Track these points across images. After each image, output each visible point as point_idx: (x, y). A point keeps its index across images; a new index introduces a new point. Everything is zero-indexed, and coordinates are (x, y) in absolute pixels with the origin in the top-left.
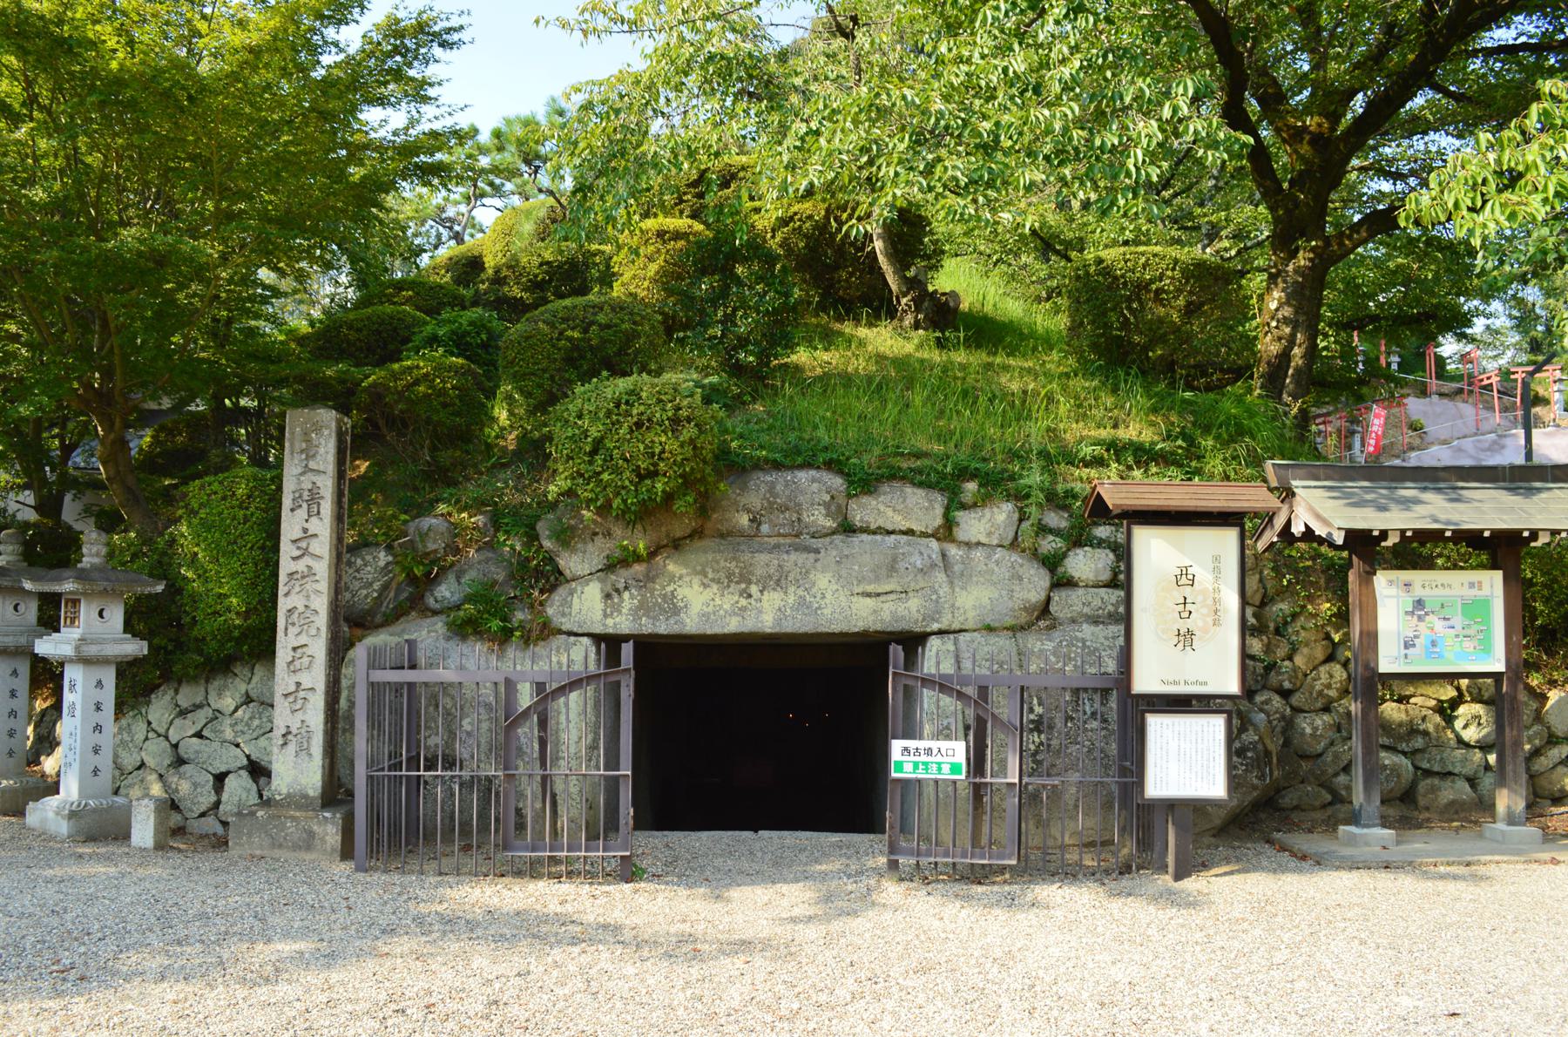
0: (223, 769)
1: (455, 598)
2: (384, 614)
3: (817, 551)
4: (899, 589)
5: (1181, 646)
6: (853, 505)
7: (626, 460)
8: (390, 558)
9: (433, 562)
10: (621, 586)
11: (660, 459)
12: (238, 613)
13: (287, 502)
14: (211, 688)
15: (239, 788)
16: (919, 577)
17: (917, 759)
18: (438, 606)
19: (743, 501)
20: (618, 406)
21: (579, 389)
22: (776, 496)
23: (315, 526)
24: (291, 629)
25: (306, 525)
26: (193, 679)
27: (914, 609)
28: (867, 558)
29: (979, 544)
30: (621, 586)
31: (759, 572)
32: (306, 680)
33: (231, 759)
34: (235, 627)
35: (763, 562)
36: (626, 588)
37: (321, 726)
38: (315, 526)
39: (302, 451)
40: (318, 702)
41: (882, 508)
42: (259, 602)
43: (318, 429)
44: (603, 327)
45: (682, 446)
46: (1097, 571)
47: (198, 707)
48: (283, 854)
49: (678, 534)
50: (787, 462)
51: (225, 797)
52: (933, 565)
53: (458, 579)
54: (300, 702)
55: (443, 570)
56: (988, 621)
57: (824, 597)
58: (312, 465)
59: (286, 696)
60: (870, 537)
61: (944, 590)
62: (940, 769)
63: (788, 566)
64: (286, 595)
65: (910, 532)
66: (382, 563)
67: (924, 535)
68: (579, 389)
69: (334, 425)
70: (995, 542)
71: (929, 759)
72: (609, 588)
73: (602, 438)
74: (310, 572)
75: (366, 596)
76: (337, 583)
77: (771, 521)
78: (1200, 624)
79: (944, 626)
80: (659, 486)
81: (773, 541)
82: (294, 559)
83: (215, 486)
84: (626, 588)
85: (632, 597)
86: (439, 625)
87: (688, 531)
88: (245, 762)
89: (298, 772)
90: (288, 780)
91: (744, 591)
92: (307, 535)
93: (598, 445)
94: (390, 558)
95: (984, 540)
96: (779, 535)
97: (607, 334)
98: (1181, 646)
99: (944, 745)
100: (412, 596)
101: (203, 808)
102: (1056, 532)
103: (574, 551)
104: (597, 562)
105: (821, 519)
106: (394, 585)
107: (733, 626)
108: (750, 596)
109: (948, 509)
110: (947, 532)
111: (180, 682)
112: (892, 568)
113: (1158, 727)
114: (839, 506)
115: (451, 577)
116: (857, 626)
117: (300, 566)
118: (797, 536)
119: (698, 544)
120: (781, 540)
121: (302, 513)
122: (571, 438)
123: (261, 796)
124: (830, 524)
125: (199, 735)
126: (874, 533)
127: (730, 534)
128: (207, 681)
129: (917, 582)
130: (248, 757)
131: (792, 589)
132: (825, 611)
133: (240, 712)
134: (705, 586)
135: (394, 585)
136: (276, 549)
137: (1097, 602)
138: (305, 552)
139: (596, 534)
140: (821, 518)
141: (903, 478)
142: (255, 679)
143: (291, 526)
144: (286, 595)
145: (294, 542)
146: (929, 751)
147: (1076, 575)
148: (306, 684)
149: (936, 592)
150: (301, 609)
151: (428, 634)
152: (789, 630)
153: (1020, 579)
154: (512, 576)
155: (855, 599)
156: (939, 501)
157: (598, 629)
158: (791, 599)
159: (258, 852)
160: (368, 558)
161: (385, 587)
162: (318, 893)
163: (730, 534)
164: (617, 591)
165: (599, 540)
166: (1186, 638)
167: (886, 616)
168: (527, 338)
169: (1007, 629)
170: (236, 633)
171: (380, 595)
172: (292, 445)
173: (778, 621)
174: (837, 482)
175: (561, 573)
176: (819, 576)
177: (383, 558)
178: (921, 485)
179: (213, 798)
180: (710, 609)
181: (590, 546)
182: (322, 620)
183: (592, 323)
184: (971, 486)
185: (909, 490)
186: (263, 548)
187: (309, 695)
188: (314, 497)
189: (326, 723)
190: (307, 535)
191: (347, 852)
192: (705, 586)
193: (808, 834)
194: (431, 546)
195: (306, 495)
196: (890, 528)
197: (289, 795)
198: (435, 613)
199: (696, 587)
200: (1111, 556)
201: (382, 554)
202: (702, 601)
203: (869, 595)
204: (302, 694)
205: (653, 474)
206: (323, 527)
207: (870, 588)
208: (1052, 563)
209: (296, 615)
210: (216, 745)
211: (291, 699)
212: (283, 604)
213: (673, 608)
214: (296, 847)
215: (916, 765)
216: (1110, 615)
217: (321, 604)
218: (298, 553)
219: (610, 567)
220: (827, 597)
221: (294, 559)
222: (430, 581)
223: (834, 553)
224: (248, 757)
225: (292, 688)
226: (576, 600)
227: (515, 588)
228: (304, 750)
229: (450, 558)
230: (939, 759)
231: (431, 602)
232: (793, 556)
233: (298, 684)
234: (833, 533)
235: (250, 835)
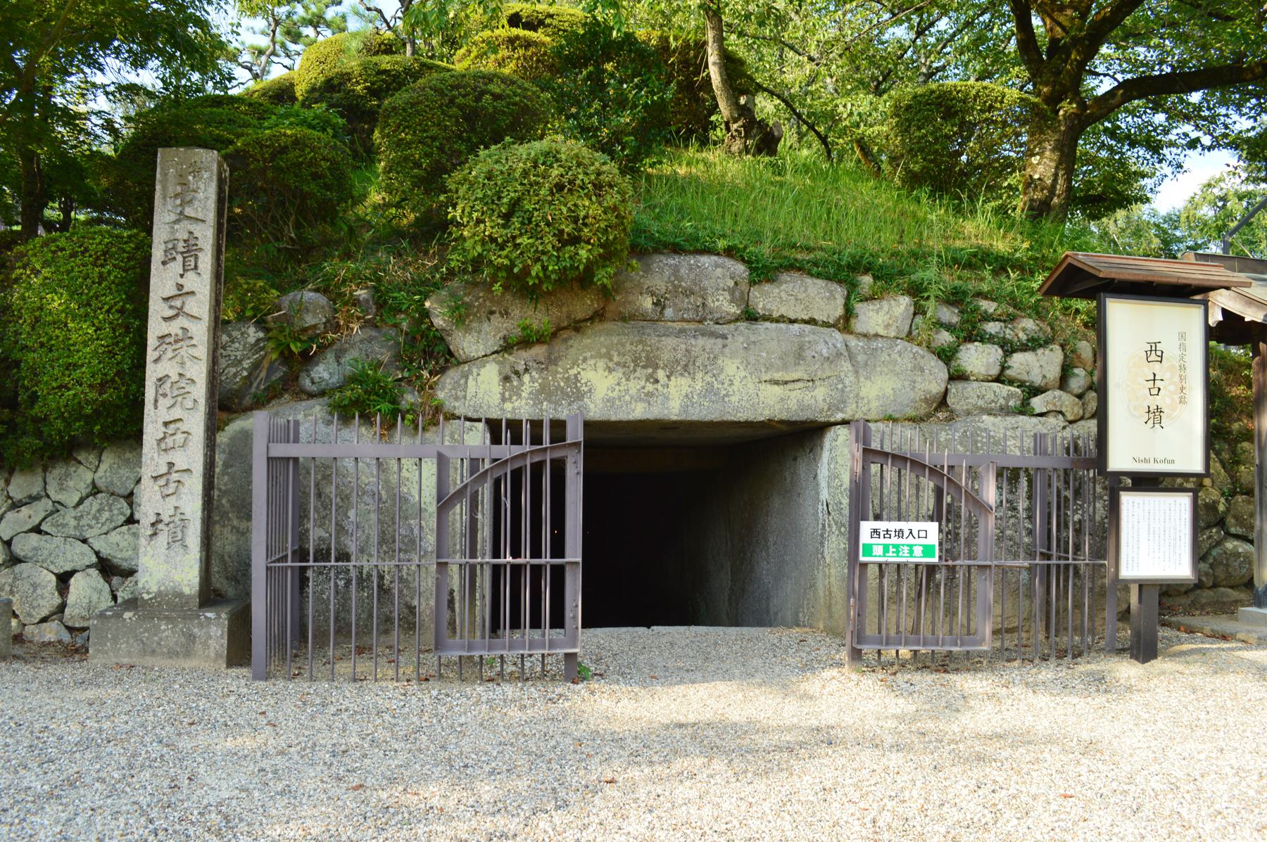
0: (68, 568)
1: (334, 380)
2: (255, 396)
3: (724, 337)
4: (806, 377)
5: (1151, 422)
6: (755, 292)
7: (548, 224)
8: (261, 335)
9: (311, 339)
10: (521, 368)
11: (585, 225)
12: (90, 386)
13: (157, 253)
14: (50, 478)
15: (86, 588)
16: (826, 365)
17: (887, 541)
18: (314, 388)
19: (647, 283)
20: (535, 166)
21: (482, 153)
22: (681, 279)
23: (191, 281)
24: (161, 400)
25: (181, 281)
26: (28, 468)
27: (820, 398)
28: (774, 344)
29: (877, 335)
30: (521, 368)
32: (180, 460)
33: (78, 556)
34: (87, 403)
35: (670, 347)
36: (526, 370)
37: (199, 514)
38: (191, 281)
39: (176, 196)
40: (195, 485)
41: (784, 295)
42: (118, 373)
43: (196, 171)
44: (496, 97)
45: (605, 213)
46: (988, 366)
47: (33, 499)
48: (158, 662)
49: (580, 316)
50: (687, 246)
51: (71, 599)
52: (839, 355)
53: (338, 359)
54: (173, 486)
55: (322, 348)
56: (890, 411)
57: (731, 384)
58: (189, 211)
59: (155, 478)
60: (774, 325)
61: (850, 380)
62: (911, 552)
63: (696, 351)
64: (156, 361)
65: (812, 321)
66: (252, 340)
67: (826, 324)
68: (482, 153)
69: (215, 166)
70: (893, 334)
71: (900, 541)
72: (507, 370)
73: (519, 199)
74: (186, 335)
75: (235, 375)
76: (215, 350)
77: (675, 305)
78: (1168, 401)
79: (847, 416)
80: (583, 253)
81: (678, 326)
82: (165, 319)
83: (62, 242)
84: (526, 370)
85: (533, 380)
86: (317, 409)
87: (590, 313)
88: (94, 559)
89: (171, 567)
91: (651, 376)
92: (182, 293)
93: (515, 205)
94: (261, 335)
95: (882, 332)
96: (683, 320)
97: (499, 104)
98: (1151, 422)
99: (916, 526)
100: (287, 372)
101: (45, 612)
102: (949, 327)
103: (468, 330)
104: (494, 343)
105: (725, 305)
106: (266, 364)
107: (639, 412)
108: (657, 381)
109: (848, 298)
110: (845, 322)
111: (11, 472)
112: (799, 356)
113: (1131, 502)
114: (742, 292)
115: (330, 356)
116: (762, 415)
117: (174, 328)
118: (700, 322)
119: (598, 327)
120: (685, 325)
121: (176, 267)
122: (481, 199)
123: (115, 598)
124: (734, 310)
125: (37, 530)
126: (777, 321)
127: (632, 317)
128: (45, 470)
129: (823, 370)
130: (97, 553)
131: (699, 375)
132: (732, 399)
133: (87, 502)
134: (610, 370)
135: (266, 364)
136: (141, 314)
137: (990, 396)
138: (180, 312)
139: (492, 313)
140: (726, 304)
141: (799, 269)
142: (103, 467)
143: (162, 281)
144: (156, 361)
145: (166, 299)
146: (900, 533)
147: (969, 369)
148: (181, 463)
149: (842, 381)
150: (175, 377)
151: (310, 417)
152: (695, 418)
153: (922, 371)
154: (398, 357)
155: (763, 386)
156: (839, 292)
158: (699, 385)
159: (125, 661)
160: (235, 334)
161: (256, 366)
162: (222, 706)
163: (632, 317)
164: (517, 373)
165: (496, 319)
166: (1155, 415)
167: (793, 404)
168: (413, 105)
169: (909, 420)
170: (88, 410)
171: (250, 375)
172: (164, 188)
173: (685, 408)
174: (740, 268)
175: (451, 354)
176: (728, 361)
177: (253, 334)
178: (818, 276)
179: (57, 600)
180: (615, 394)
181: (486, 327)
182: (200, 391)
183: (483, 93)
184: (867, 280)
185: (809, 281)
186: (122, 311)
187: (184, 477)
188: (191, 249)
189: (204, 510)
190: (182, 293)
191: (239, 652)
192: (610, 370)
193: (630, 629)
194: (310, 320)
195: (181, 246)
196: (792, 316)
197: (159, 594)
198: (311, 396)
199: (600, 371)
200: (1000, 351)
201: (252, 330)
202: (606, 386)
203: (777, 383)
204: (175, 476)
205: (575, 240)
206: (201, 284)
207: (778, 376)
208: (946, 356)
209: (168, 385)
210: (58, 541)
211: (162, 482)
212: (152, 372)
213: (577, 393)
214: (172, 654)
215: (886, 548)
216: (1002, 409)
217: (199, 372)
218: (171, 313)
219: (507, 347)
220: (733, 384)
221: (165, 319)
222: (307, 359)
223: (741, 339)
224: (97, 553)
225: (164, 469)
226: (471, 382)
227: (402, 370)
228: (177, 541)
229: (330, 335)
230: (911, 540)
231: (307, 383)
232: (701, 341)
233: (171, 465)
234: (737, 320)
235: (115, 640)
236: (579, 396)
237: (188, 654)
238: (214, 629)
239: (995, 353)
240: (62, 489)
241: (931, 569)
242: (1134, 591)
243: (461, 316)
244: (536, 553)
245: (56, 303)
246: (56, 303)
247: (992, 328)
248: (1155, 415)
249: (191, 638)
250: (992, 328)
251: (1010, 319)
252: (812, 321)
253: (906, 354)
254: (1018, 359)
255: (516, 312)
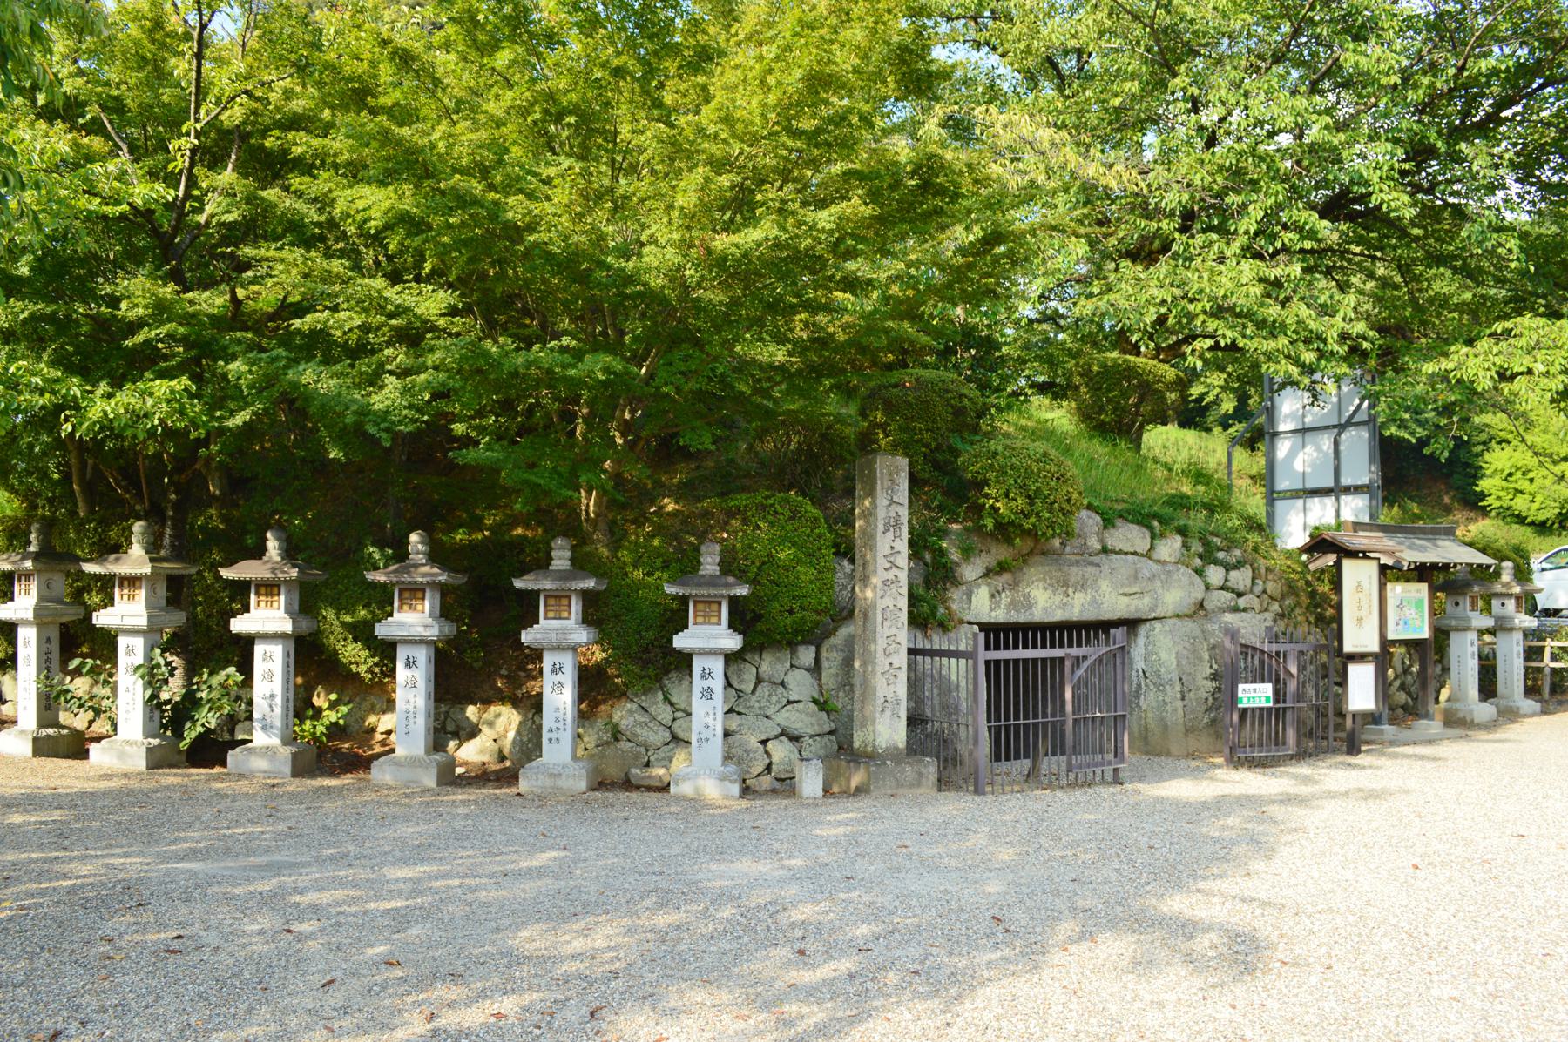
31: (1073, 579)
35: (1075, 572)
65: (1135, 553)
81: (1073, 558)
90: (886, 736)
92: (894, 552)
104: (980, 571)
121: (890, 535)
157: (985, 620)
167: (1132, 608)
181: (978, 561)
188: (897, 524)
190: (894, 552)
207: (1127, 590)
214: (912, 786)
219: (988, 573)
236: (1030, 606)
237: (919, 785)
238: (930, 768)
239: (1221, 571)
240: (742, 681)
241: (1269, 709)
242: (44, 732)
243: (967, 553)
244: (1035, 716)
245: (784, 554)
246: (784, 554)
247: (1221, 555)
248: (1360, 620)
249: (920, 774)
250: (1221, 555)
251: (1228, 550)
252: (1135, 553)
253: (1185, 574)
254: (1233, 574)
255: (993, 551)
